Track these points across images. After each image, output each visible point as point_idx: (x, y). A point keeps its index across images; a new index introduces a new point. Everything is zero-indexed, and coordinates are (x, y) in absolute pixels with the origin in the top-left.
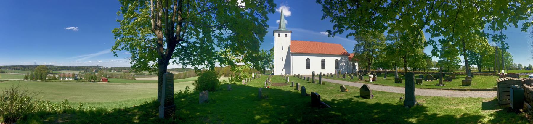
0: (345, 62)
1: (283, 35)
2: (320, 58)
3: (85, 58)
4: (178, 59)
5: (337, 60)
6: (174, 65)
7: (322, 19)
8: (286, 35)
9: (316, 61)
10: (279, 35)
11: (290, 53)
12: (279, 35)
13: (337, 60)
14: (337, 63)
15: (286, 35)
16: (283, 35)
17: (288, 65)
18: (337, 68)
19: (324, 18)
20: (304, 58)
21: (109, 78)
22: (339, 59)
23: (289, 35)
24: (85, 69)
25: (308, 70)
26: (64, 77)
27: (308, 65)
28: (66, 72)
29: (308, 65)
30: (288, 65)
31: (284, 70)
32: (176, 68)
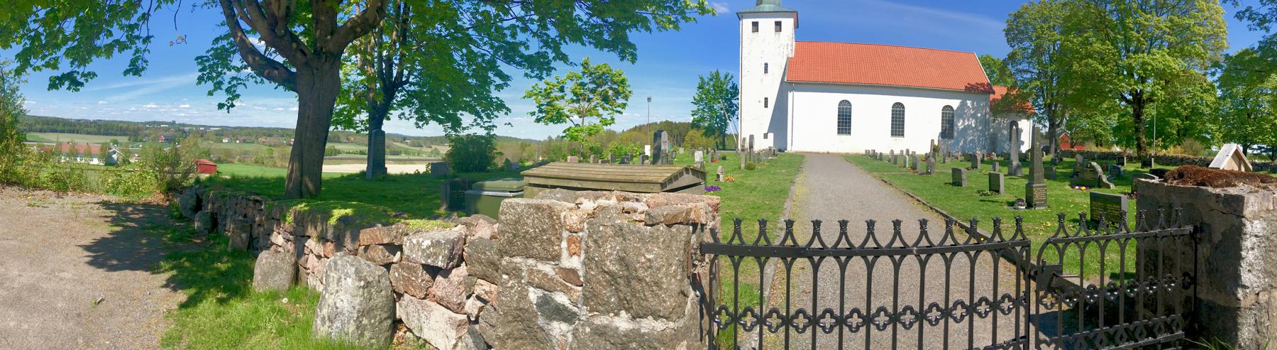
0: (974, 116)
1: (767, 24)
2: (889, 101)
3: (141, 92)
4: (406, 110)
5: (947, 108)
6: (397, 124)
7: (126, 72)
8: (778, 24)
9: (872, 111)
10: (755, 25)
11: (795, 80)
12: (755, 25)
13: (947, 108)
14: (949, 118)
15: (778, 24)
16: (767, 24)
17: (779, 123)
18: (948, 130)
19: (222, 25)
20: (831, 101)
21: (220, 161)
22: (955, 104)
23: (788, 23)
24: (133, 131)
25: (844, 137)
26: (74, 153)
27: (844, 123)
28: (81, 140)
29: (844, 123)
30: (779, 123)
31: (771, 136)
32: (252, 176)
